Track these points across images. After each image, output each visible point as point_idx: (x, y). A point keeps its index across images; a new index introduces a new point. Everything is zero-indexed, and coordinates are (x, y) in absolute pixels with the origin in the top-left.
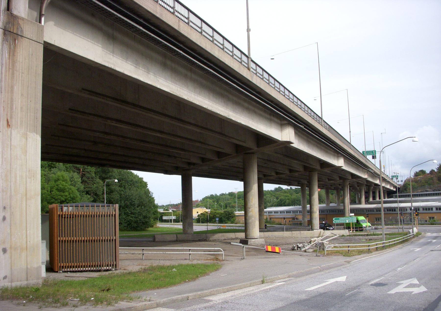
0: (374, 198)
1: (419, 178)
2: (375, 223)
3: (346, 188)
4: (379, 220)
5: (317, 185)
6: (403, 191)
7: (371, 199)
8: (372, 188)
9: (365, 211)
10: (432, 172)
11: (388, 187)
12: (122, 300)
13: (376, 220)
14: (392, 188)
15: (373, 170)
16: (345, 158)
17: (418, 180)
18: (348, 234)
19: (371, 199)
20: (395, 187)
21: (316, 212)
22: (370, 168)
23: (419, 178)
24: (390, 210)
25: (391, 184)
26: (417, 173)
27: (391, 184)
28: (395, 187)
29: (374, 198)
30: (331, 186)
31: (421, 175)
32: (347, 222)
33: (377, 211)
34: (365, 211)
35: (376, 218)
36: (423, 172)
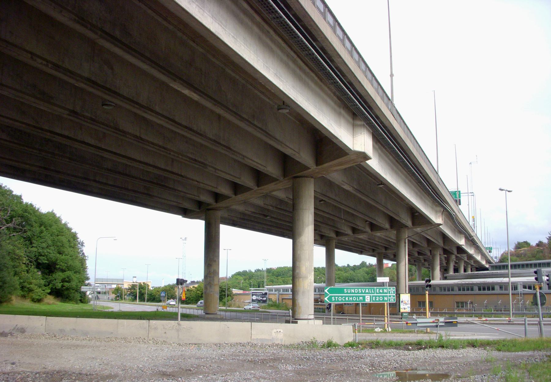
0: (456, 270)
1: (522, 251)
2: (456, 311)
3: (402, 245)
4: (463, 307)
5: (312, 210)
6: (501, 265)
7: (451, 273)
8: (453, 257)
9: (438, 289)
10: (540, 244)
11: (479, 258)
12: (462, 314)
13: (458, 307)
14: (484, 263)
15: (454, 212)
16: (377, 139)
17: (522, 254)
18: (350, 340)
19: (451, 273)
20: (488, 262)
21: (306, 278)
22: (447, 203)
23: (522, 251)
24: (484, 289)
25: (483, 255)
26: (519, 243)
27: (483, 255)
28: (488, 262)
29: (456, 270)
30: (386, 248)
31: (524, 247)
32: (368, 300)
33: (459, 290)
34: (438, 289)
35: (457, 303)
36: (526, 243)
